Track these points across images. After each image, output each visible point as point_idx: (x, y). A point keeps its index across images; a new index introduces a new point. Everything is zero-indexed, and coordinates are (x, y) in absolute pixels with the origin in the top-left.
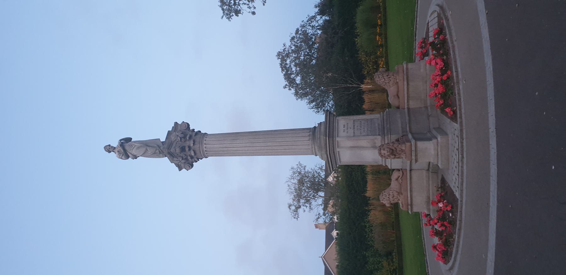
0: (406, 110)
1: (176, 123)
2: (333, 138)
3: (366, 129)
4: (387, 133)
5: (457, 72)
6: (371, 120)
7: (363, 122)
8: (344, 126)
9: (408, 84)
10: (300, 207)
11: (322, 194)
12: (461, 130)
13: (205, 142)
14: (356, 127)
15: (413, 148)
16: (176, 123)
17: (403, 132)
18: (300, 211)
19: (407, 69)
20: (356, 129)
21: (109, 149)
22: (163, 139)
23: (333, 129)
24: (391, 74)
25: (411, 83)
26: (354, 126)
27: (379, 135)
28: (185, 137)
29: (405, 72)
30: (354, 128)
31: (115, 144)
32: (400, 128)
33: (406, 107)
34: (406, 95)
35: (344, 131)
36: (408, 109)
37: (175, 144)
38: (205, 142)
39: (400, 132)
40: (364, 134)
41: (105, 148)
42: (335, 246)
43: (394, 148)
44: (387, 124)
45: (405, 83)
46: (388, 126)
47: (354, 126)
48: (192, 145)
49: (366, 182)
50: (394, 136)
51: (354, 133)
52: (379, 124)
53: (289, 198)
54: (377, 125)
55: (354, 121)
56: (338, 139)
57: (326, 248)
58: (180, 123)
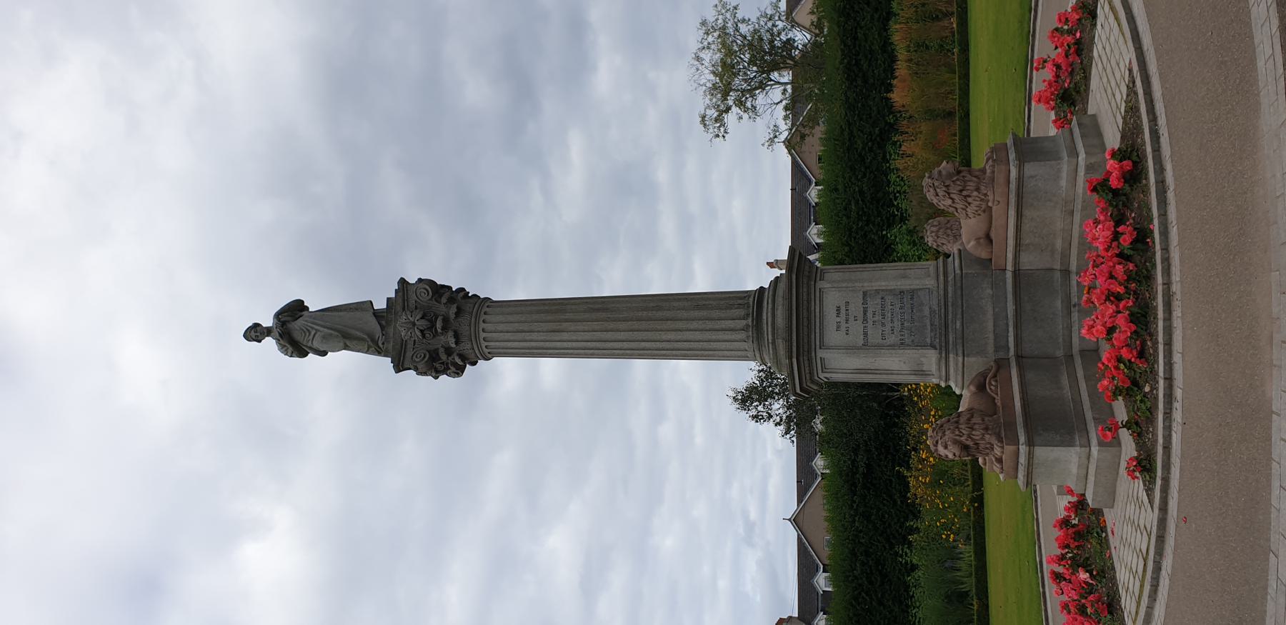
0: (1009, 275)
1: (403, 282)
2: (809, 352)
3: (897, 324)
4: (955, 345)
5: (1169, 379)
6: (913, 292)
7: (889, 299)
8: (838, 309)
9: (1019, 215)
10: (728, 109)
11: (786, 77)
12: (1162, 522)
13: (483, 335)
14: (870, 315)
15: (1022, 460)
16: (403, 282)
17: (997, 349)
18: (730, 118)
19: (1020, 179)
20: (870, 322)
21: (255, 333)
22: (380, 304)
23: (809, 327)
24: (971, 186)
25: (1028, 213)
26: (865, 312)
27: (934, 347)
28: (432, 326)
29: (1013, 186)
30: (865, 320)
31: (268, 322)
32: (991, 336)
33: (1010, 267)
34: (1011, 242)
35: (838, 328)
36: (1017, 273)
37: (410, 345)
38: (483, 335)
39: (991, 348)
40: (892, 339)
41: (245, 336)
42: (820, 493)
43: (970, 443)
44: (955, 315)
45: (1012, 213)
46: (958, 324)
47: (865, 312)
48: (452, 316)
49: (893, 59)
50: (972, 359)
51: (866, 334)
52: (932, 311)
53: (701, 102)
54: (927, 312)
55: (865, 294)
56: (821, 354)
57: (799, 501)
58: (412, 280)
